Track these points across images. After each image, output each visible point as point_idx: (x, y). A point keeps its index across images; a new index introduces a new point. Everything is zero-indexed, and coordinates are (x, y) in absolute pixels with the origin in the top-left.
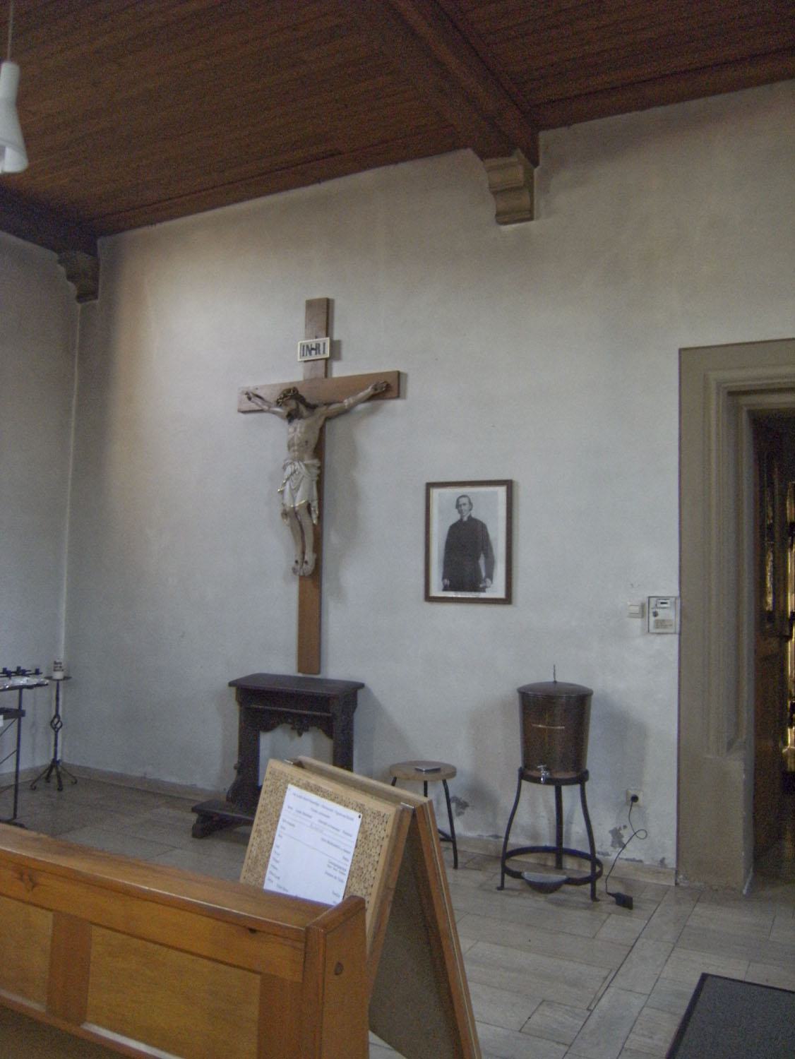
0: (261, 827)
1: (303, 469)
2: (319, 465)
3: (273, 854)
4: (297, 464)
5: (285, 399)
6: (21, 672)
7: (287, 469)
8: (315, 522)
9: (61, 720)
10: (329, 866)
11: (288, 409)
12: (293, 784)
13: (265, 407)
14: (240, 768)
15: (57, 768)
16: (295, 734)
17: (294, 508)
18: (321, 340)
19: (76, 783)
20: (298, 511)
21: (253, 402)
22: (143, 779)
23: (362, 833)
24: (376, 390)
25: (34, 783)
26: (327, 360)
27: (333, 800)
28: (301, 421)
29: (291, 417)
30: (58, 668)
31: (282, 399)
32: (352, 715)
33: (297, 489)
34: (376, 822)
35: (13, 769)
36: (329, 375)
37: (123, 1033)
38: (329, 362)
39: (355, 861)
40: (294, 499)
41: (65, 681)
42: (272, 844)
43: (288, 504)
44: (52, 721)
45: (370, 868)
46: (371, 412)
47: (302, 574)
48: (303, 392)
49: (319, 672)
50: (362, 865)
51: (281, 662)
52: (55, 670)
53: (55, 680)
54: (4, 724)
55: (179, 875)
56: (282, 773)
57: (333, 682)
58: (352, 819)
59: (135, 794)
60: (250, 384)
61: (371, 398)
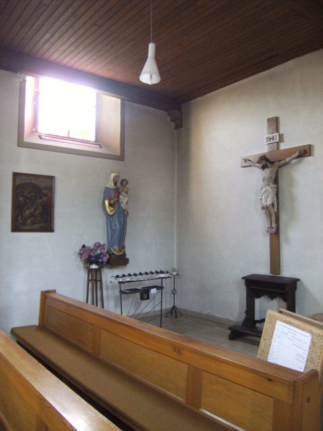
0: (265, 337)
1: (270, 189)
2: (276, 187)
3: (271, 349)
4: (267, 187)
5: (261, 160)
6: (161, 272)
7: (263, 190)
8: (276, 211)
9: (176, 291)
10: (297, 356)
11: (262, 164)
12: (279, 320)
13: (252, 164)
14: (247, 312)
15: (175, 309)
16: (270, 299)
17: (267, 205)
18: (274, 135)
19: (182, 315)
20: (269, 206)
21: (247, 163)
22: (208, 315)
23: (312, 343)
24: (300, 153)
26: (277, 142)
27: (298, 328)
28: (268, 169)
29: (264, 168)
31: (260, 160)
32: (295, 292)
33: (268, 197)
34: (318, 338)
35: (160, 309)
36: (279, 149)
37: (216, 414)
38: (278, 143)
39: (309, 354)
40: (266, 202)
41: (177, 276)
42: (270, 345)
43: (264, 204)
44: (173, 291)
45: (316, 358)
46: (299, 163)
47: (271, 233)
48: (268, 157)
49: (279, 274)
50: (312, 356)
51: (263, 269)
52: (173, 272)
54: (157, 291)
55: (233, 354)
56: (274, 315)
57: (284, 278)
58: (307, 337)
59: (204, 321)
60: (246, 155)
61: (298, 157)
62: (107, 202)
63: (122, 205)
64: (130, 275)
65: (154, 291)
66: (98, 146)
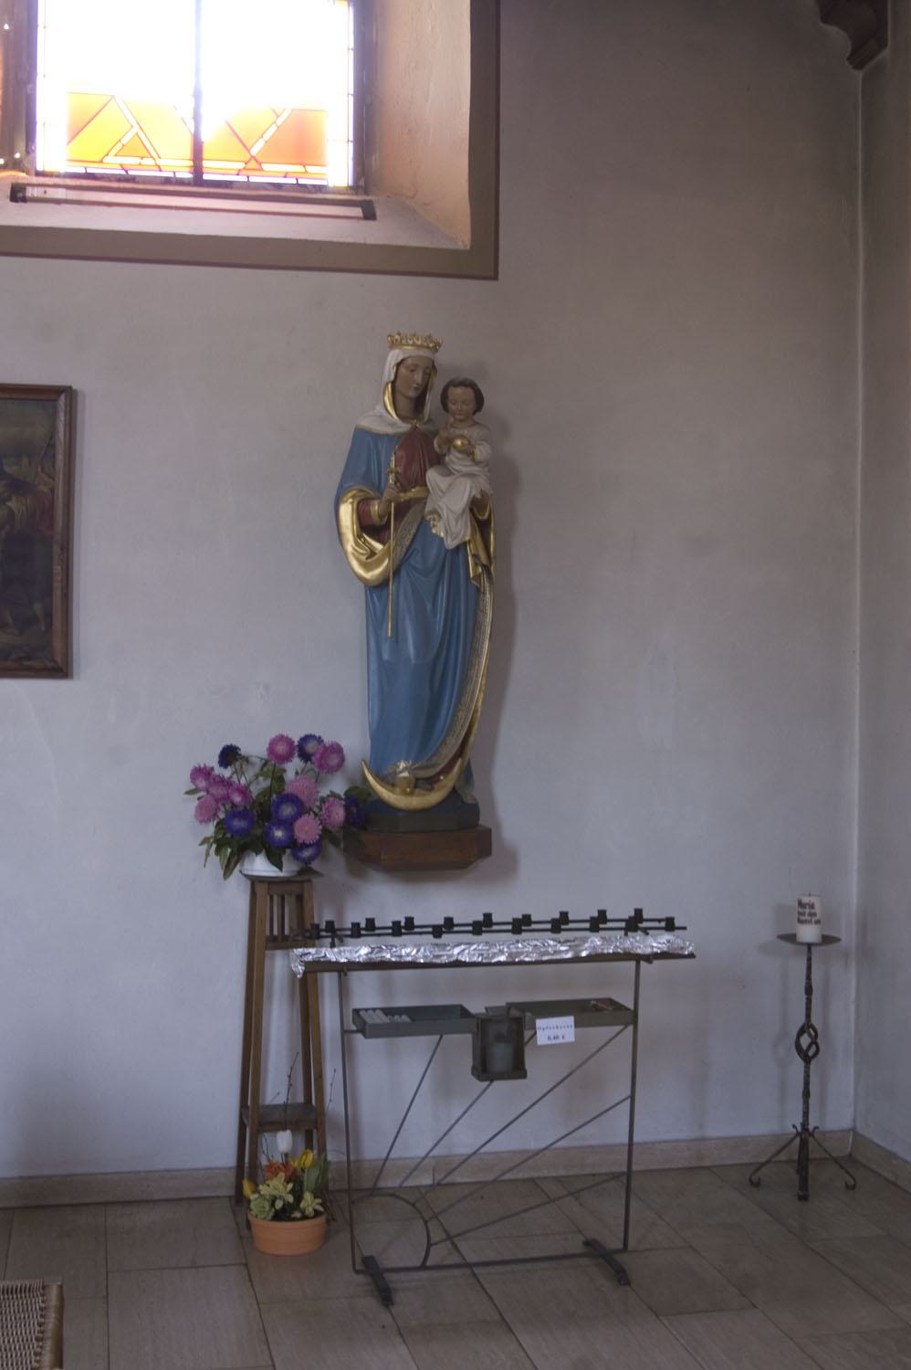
19: (853, 1187)
25: (758, 1169)
30: (807, 917)
53: (802, 944)
62: (346, 512)
63: (439, 530)
64: (559, 924)
65: (559, 1032)
66: (358, 212)
